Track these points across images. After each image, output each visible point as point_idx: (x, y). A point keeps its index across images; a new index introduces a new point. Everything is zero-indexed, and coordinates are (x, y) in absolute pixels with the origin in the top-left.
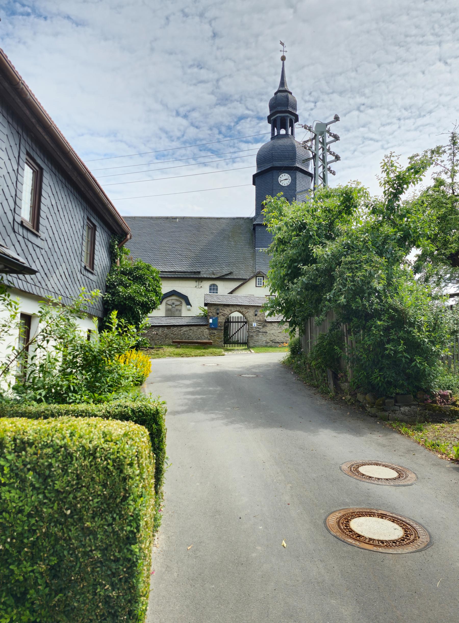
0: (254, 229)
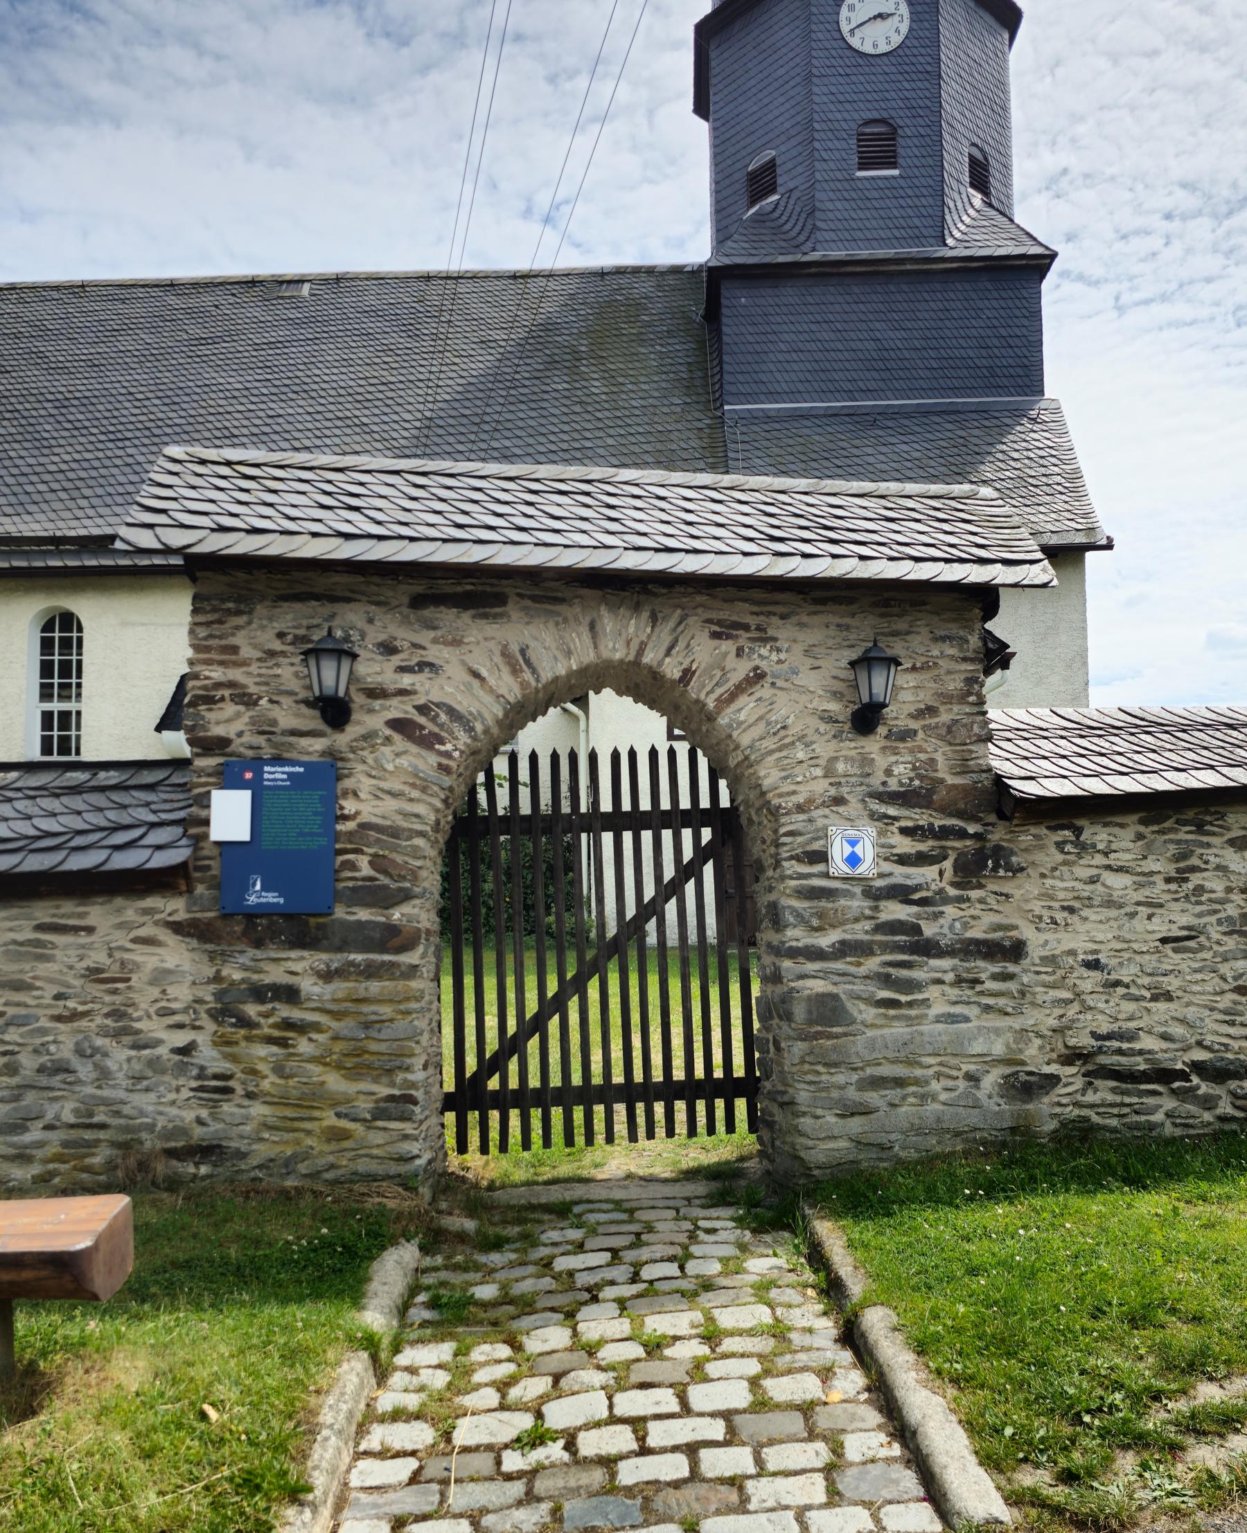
0: (713, 313)
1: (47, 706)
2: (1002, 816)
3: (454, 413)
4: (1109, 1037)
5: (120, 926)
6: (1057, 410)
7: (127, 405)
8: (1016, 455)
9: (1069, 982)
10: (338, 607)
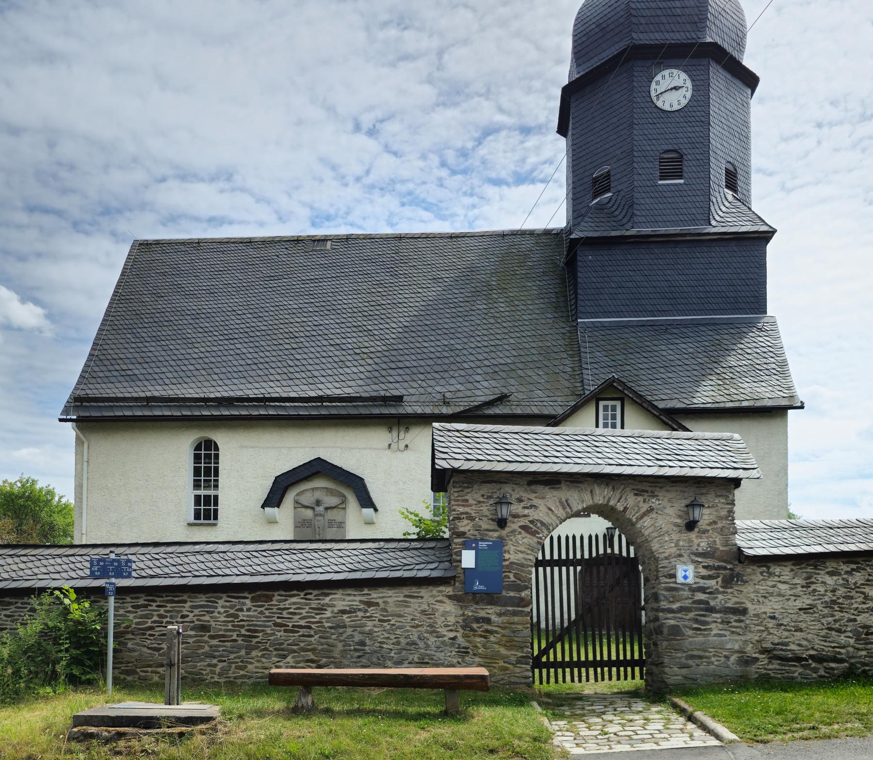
0: (571, 263)
1: (198, 492)
2: (740, 562)
3: (420, 323)
4: (778, 644)
5: (431, 596)
6: (774, 323)
7: (233, 317)
8: (749, 351)
9: (764, 624)
10: (502, 486)
